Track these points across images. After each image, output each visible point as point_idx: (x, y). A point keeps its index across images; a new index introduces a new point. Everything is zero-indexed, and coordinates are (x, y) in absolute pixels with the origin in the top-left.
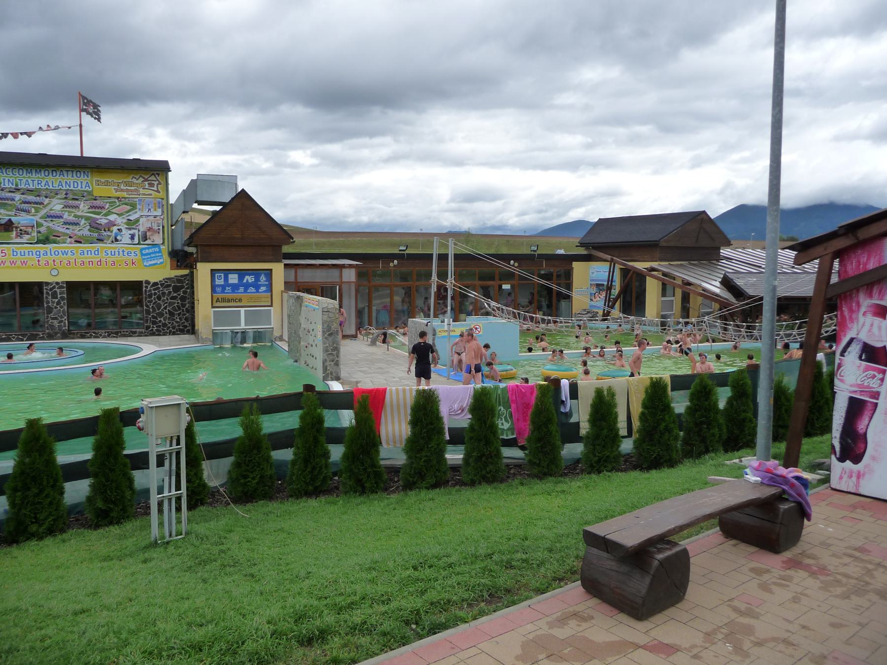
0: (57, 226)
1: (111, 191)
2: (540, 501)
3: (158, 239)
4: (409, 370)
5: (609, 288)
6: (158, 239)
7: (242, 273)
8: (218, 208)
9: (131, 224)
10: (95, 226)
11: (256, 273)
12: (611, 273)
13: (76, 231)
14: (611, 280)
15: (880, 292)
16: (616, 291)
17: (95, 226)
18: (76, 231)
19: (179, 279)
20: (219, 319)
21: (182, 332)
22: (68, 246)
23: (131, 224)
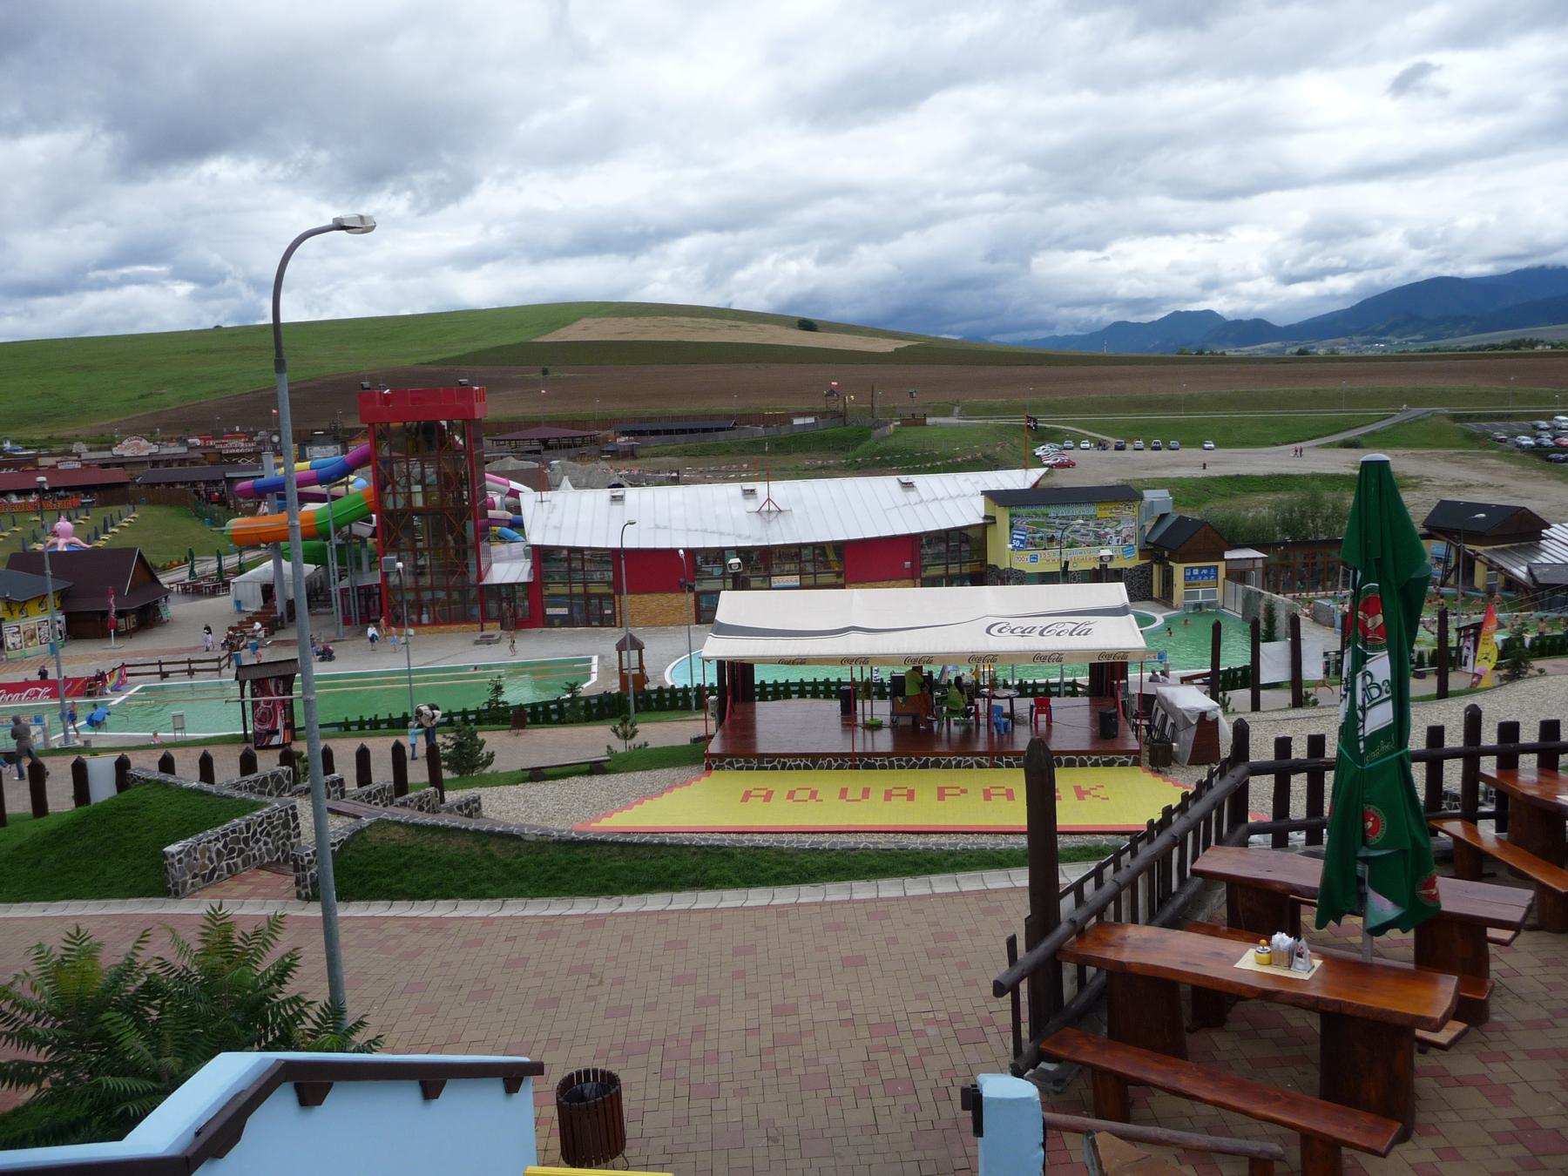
0: (1077, 537)
1: (1107, 514)
2: (679, 725)
3: (1132, 541)
4: (739, 536)
5: (1446, 562)
6: (1132, 541)
7: (1201, 568)
8: (811, 420)
9: (1118, 533)
10: (1098, 536)
11: (1209, 568)
12: (1448, 550)
13: (1087, 539)
14: (1448, 555)
15: (1291, 130)
16: (1452, 564)
17: (1098, 536)
18: (1087, 539)
19: (1144, 566)
20: (1188, 595)
21: (1144, 599)
22: (1083, 548)
23: (1118, 533)
